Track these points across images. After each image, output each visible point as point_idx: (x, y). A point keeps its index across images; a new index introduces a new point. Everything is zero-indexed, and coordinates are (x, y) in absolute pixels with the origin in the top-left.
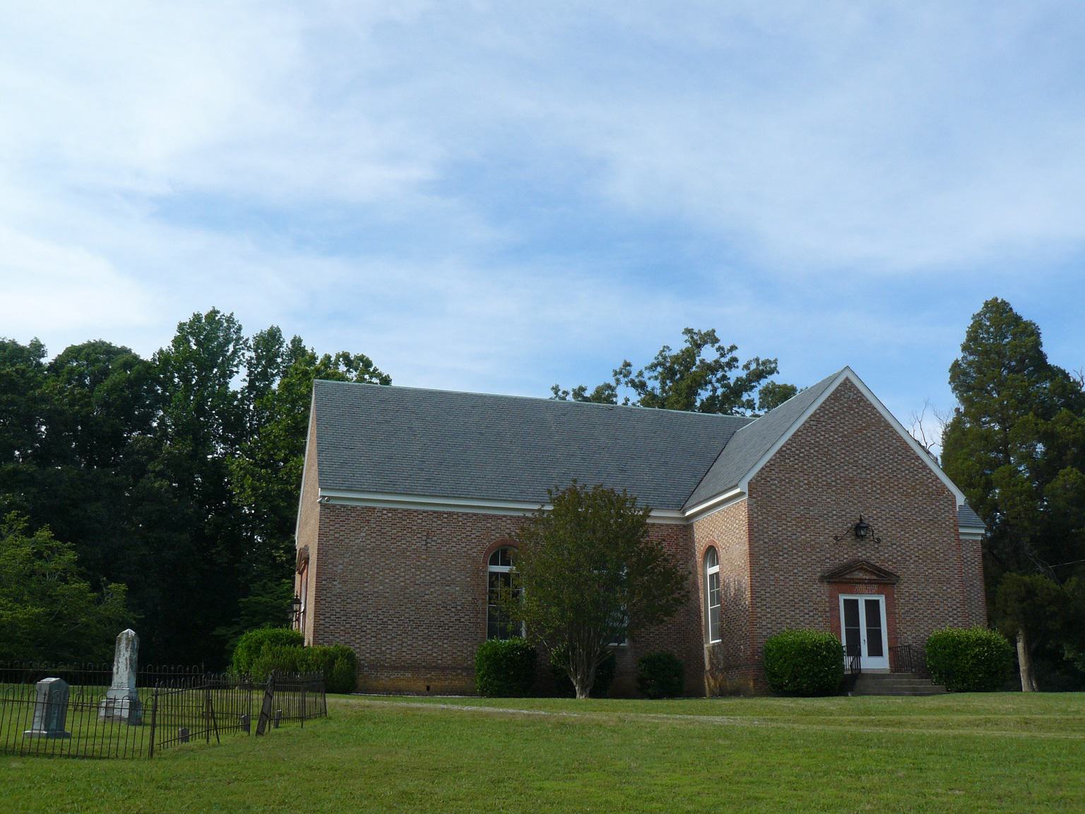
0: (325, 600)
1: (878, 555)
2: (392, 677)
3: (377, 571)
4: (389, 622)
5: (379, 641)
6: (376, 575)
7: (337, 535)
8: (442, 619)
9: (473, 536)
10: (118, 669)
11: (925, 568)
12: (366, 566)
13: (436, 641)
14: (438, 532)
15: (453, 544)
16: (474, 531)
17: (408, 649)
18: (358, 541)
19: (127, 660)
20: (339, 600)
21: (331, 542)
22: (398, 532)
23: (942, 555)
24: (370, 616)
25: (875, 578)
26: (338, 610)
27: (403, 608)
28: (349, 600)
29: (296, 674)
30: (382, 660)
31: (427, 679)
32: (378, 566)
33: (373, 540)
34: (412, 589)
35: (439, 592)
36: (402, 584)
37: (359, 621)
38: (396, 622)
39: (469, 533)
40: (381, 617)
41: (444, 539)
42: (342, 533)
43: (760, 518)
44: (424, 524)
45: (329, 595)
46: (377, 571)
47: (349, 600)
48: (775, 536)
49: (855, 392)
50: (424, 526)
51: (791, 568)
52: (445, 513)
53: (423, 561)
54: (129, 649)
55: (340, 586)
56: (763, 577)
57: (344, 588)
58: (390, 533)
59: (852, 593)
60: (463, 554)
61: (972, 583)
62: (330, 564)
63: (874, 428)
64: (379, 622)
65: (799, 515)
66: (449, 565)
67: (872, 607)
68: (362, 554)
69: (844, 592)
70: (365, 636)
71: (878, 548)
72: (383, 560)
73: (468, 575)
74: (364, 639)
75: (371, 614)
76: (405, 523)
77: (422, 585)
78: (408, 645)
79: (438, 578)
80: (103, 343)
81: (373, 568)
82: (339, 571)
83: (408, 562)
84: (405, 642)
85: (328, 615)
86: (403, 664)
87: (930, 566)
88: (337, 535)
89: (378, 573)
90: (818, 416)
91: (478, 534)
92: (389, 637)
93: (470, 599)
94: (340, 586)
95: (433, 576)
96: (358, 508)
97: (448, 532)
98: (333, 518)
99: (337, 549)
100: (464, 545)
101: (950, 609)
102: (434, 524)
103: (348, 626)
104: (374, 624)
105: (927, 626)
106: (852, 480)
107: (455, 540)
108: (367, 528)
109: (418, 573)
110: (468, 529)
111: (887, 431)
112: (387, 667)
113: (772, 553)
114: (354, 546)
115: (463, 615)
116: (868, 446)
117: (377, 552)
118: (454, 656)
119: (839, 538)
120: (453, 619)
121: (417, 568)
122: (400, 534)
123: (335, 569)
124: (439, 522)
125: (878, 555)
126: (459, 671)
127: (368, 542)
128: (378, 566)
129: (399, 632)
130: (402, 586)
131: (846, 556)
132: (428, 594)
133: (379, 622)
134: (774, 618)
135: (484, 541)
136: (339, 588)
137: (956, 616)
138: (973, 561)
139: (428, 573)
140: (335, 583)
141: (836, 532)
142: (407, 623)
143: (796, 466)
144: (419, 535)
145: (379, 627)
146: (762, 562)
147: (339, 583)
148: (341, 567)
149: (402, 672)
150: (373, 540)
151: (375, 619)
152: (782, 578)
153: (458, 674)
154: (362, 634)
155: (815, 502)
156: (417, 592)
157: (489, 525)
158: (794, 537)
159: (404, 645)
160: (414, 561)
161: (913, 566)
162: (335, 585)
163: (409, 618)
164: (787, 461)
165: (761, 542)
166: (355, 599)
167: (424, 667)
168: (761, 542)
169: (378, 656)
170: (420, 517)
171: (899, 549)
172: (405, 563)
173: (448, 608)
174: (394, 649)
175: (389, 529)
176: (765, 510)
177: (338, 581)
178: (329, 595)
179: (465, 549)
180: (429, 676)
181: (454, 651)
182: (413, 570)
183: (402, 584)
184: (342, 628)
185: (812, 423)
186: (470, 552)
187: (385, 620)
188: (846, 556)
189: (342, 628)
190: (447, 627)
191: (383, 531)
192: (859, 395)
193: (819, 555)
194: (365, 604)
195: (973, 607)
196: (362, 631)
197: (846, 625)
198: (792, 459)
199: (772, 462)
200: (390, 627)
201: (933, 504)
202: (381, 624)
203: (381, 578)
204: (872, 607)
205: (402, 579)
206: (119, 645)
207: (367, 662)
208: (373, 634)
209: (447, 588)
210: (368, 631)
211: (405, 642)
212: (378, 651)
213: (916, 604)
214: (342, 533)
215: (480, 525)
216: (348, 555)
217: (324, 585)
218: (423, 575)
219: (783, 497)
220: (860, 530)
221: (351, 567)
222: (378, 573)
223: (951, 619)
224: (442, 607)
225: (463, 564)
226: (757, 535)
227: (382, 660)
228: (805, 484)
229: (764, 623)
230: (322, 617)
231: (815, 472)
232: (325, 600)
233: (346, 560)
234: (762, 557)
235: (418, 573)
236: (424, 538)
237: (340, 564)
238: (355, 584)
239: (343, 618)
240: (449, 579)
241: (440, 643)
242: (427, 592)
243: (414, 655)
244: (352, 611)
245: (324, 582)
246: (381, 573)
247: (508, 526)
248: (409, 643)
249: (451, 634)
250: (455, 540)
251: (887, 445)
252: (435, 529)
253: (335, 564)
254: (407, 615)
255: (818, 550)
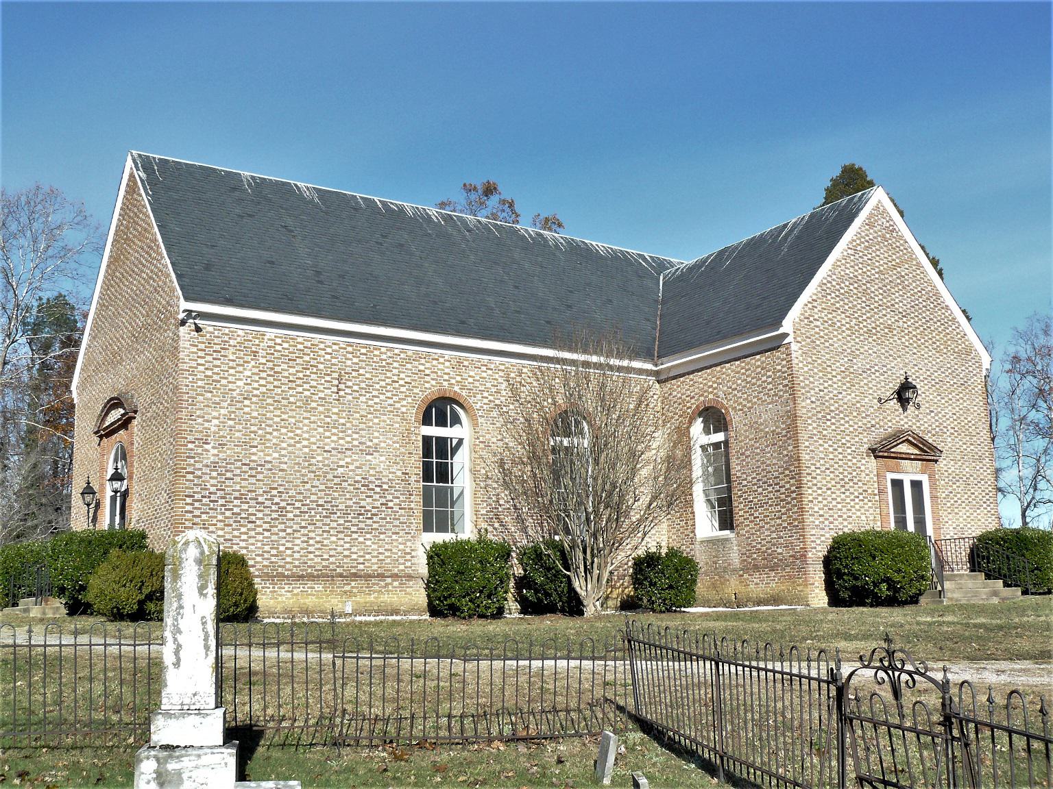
0: (193, 473)
1: (918, 424)
2: (295, 591)
3: (269, 430)
4: (289, 508)
5: (274, 538)
6: (268, 436)
7: (209, 373)
8: (363, 503)
9: (402, 382)
10: (177, 653)
11: (961, 443)
12: (253, 421)
13: (355, 536)
14: (354, 374)
15: (375, 393)
16: (402, 376)
17: (316, 549)
18: (240, 383)
19: (204, 623)
20: (214, 474)
21: (200, 383)
22: (297, 371)
24: (261, 499)
25: (918, 453)
26: (213, 489)
27: (308, 486)
28: (229, 475)
30: (279, 566)
31: (345, 592)
32: (270, 422)
33: (263, 382)
34: (320, 458)
35: (357, 464)
36: (306, 450)
37: (245, 507)
38: (298, 508)
39: (395, 378)
40: (277, 500)
41: (363, 385)
42: (216, 370)
43: (806, 369)
44: (334, 361)
45: (198, 465)
46: (269, 430)
47: (229, 475)
48: (822, 393)
49: (888, 218)
50: (335, 365)
51: (839, 437)
53: (335, 417)
54: (211, 590)
55: (215, 451)
56: (812, 448)
57: (221, 455)
58: (286, 374)
60: (389, 408)
62: (198, 417)
63: (907, 266)
64: (274, 508)
65: (843, 369)
66: (371, 424)
67: (917, 485)
68: (247, 402)
70: (255, 530)
71: (918, 416)
72: (278, 412)
73: (395, 438)
74: (252, 533)
75: (262, 495)
76: (307, 358)
77: (334, 452)
78: (318, 542)
79: (356, 443)
81: (263, 425)
82: (213, 429)
83: (312, 418)
84: (312, 538)
85: (197, 496)
86: (309, 571)
88: (209, 373)
89: (271, 433)
90: (854, 244)
91: (408, 380)
92: (289, 531)
94: (215, 451)
95: (348, 439)
97: (368, 376)
98: (202, 346)
99: (209, 395)
100: (389, 394)
102: (349, 363)
103: (228, 514)
104: (267, 511)
106: (889, 327)
107: (377, 386)
109: (328, 434)
110: (395, 371)
111: (918, 272)
112: (288, 577)
113: (820, 416)
114: (234, 390)
115: (390, 497)
116: (903, 287)
117: (270, 401)
118: (381, 557)
119: (883, 401)
120: (378, 504)
121: (327, 427)
122: (301, 375)
123: (206, 425)
124: (355, 360)
125: (918, 424)
126: (389, 580)
128: (270, 422)
129: (303, 524)
130: (306, 453)
131: (890, 424)
132: (342, 466)
133: (274, 508)
134: (825, 502)
135: (416, 391)
136: (213, 455)
139: (341, 435)
140: (206, 446)
141: (879, 392)
142: (314, 509)
143: (838, 305)
144: (328, 378)
145: (274, 515)
146: (810, 428)
148: (215, 422)
149: (310, 584)
150: (263, 382)
151: (268, 503)
152: (831, 449)
154: (250, 526)
155: (858, 352)
156: (326, 462)
157: (422, 368)
158: (840, 397)
159: (311, 542)
160: (322, 417)
162: (207, 451)
163: (317, 501)
164: (829, 297)
165: (808, 401)
166: (238, 472)
167: (341, 575)
168: (808, 401)
169: (273, 559)
170: (329, 350)
172: (309, 419)
173: (371, 487)
174: (296, 548)
176: (810, 360)
177: (212, 444)
178: (198, 465)
179: (391, 401)
180: (347, 588)
181: (381, 550)
182: (321, 430)
183: (306, 450)
184: (220, 517)
185: (849, 251)
186: (398, 405)
187: (283, 504)
188: (890, 424)
189: (220, 517)
190: (369, 516)
191: (277, 369)
192: (892, 223)
193: (865, 421)
194: (253, 480)
196: (249, 522)
197: (895, 513)
198: (833, 295)
199: (814, 297)
200: (290, 515)
202: (277, 511)
203: (274, 441)
204: (917, 485)
205: (305, 443)
206: (176, 576)
207: (257, 570)
208: (266, 526)
209: (369, 457)
210: (258, 523)
211: (312, 538)
212: (274, 552)
213: (954, 486)
214: (216, 370)
215: (409, 366)
216: (225, 404)
217: (191, 450)
218: (335, 438)
219: (827, 344)
220: (905, 392)
221: (231, 423)
222: (271, 433)
224: (363, 486)
225: (388, 422)
226: (803, 391)
227: (279, 566)
228: (847, 329)
229: (816, 509)
231: (856, 315)
232: (193, 473)
233: (223, 411)
234: (810, 421)
235: (328, 434)
236: (336, 382)
237: (214, 418)
238: (238, 449)
239: (221, 502)
240: (370, 444)
241: (361, 539)
242: (341, 463)
243: (326, 556)
244: (233, 491)
245: (190, 446)
246: (275, 433)
247: (447, 371)
248: (318, 539)
249: (375, 526)
250: (377, 386)
251: (919, 289)
252: (348, 370)
253: (206, 417)
254: (314, 498)
255: (864, 415)
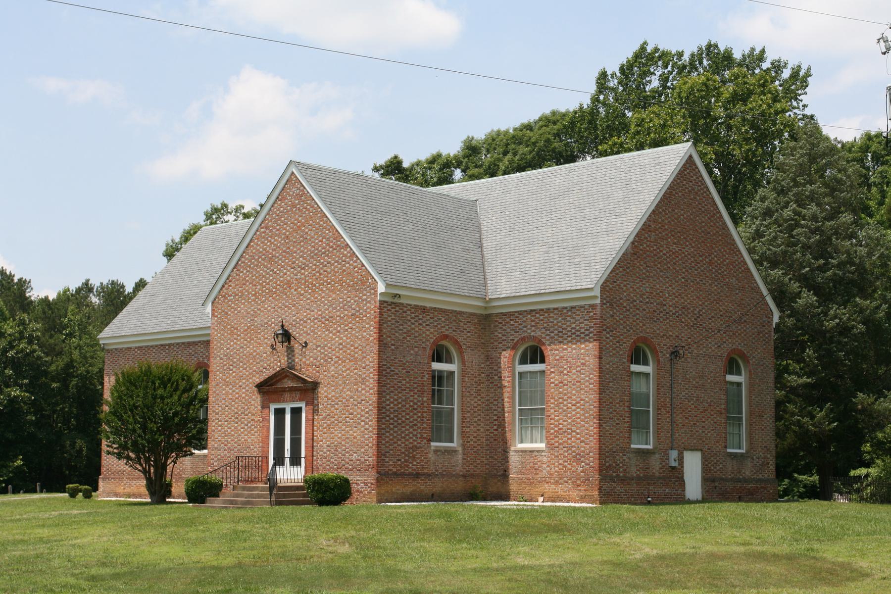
23: (360, 352)
29: (870, 445)
59: (279, 401)
61: (583, 361)
67: (296, 412)
69: (274, 401)
80: (498, 133)
87: (348, 366)
101: (363, 413)
105: (340, 433)
137: (367, 420)
138: (587, 332)
161: (333, 368)
171: (322, 351)
195: (582, 392)
201: (356, 297)
223: (363, 423)
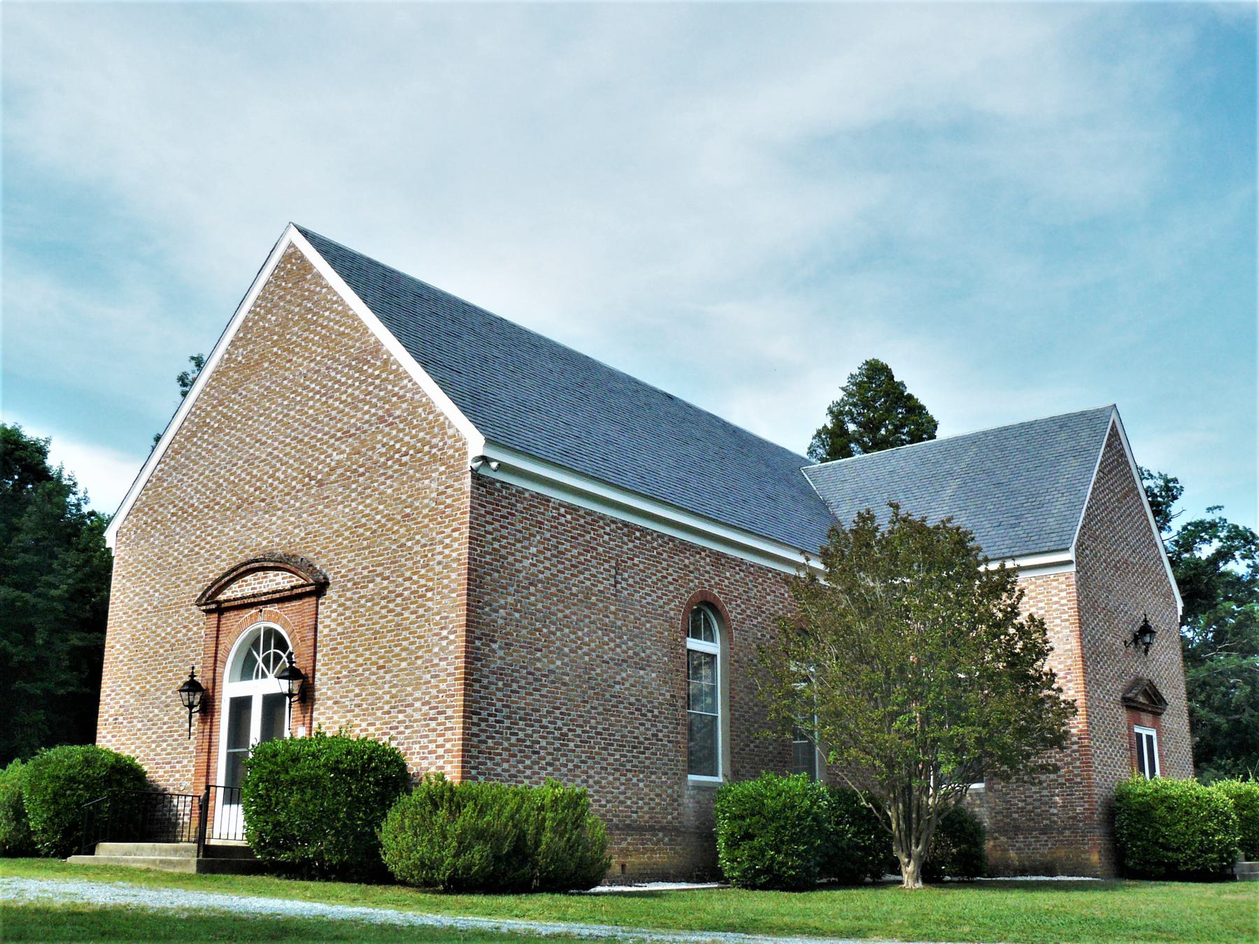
13: (630, 775)
18: (527, 563)
52: (639, 530)
67: (1150, 738)
82: (500, 622)
93: (668, 696)
96: (527, 495)
108: (538, 537)
127: (541, 567)
147: (500, 648)
153: (659, 841)
175: (568, 546)
204: (1150, 738)
230: (475, 719)
